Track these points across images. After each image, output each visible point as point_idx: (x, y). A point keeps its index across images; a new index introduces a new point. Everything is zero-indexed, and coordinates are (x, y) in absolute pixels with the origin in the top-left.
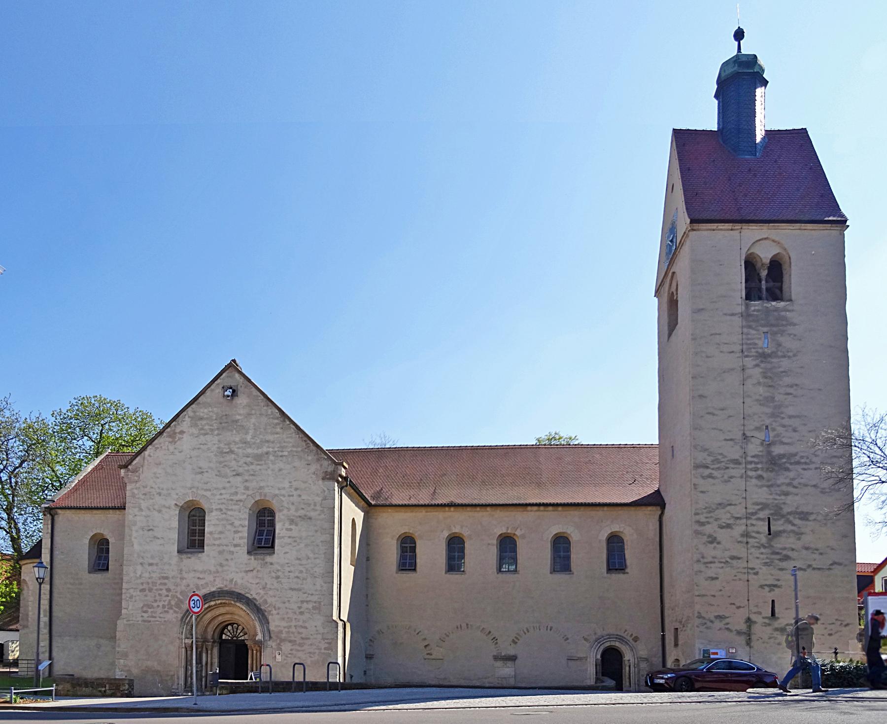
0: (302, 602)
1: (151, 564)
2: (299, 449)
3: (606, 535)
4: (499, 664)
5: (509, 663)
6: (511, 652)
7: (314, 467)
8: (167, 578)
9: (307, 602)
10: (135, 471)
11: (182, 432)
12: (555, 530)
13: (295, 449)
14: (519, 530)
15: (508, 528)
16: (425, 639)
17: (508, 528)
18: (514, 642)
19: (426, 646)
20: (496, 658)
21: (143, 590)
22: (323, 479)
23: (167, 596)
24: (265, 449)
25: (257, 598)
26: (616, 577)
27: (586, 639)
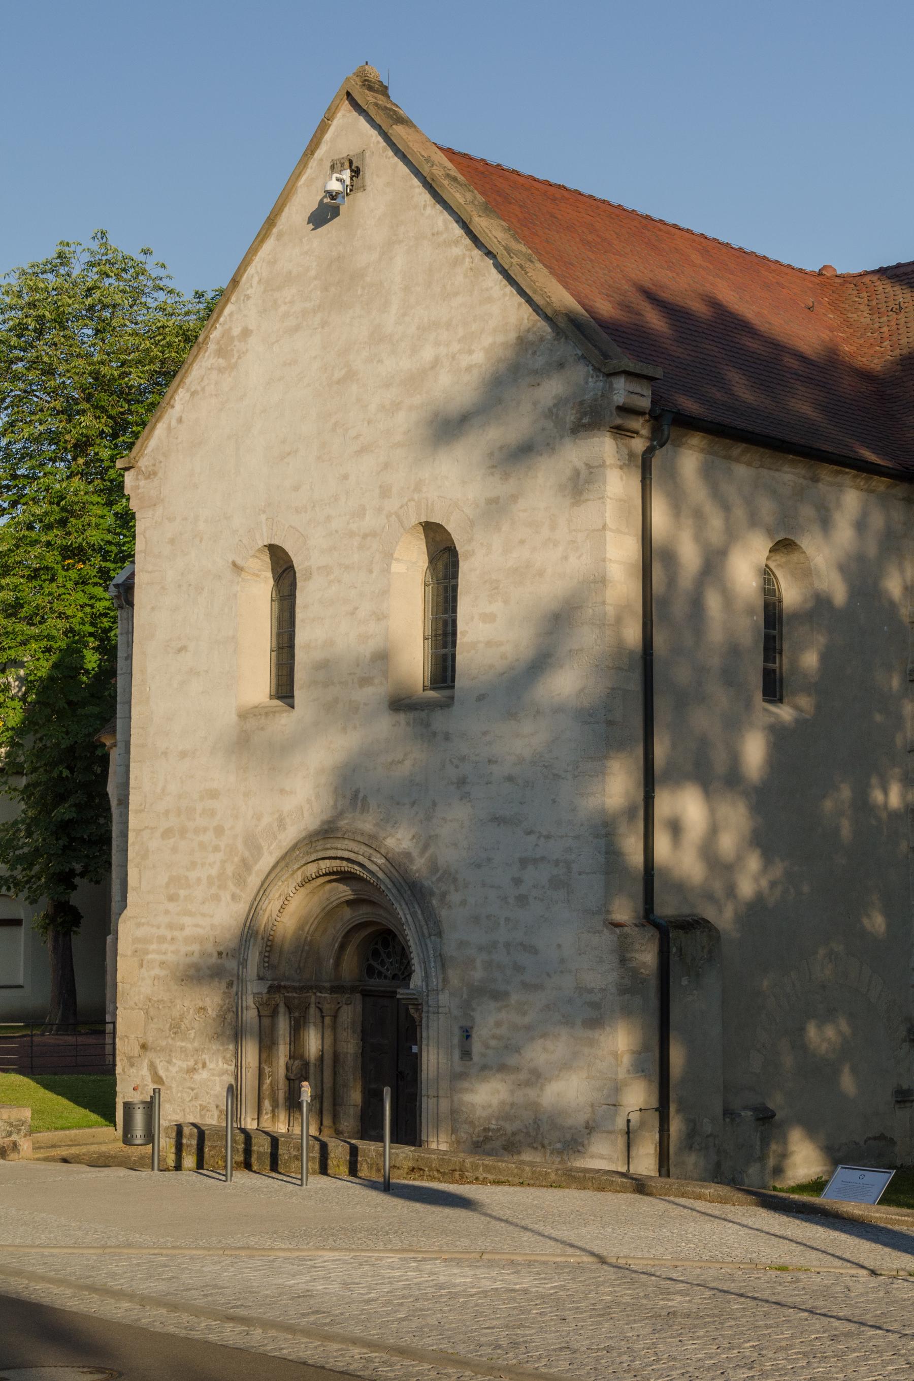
0: (524, 862)
1: (183, 755)
8: (213, 794)
9: (535, 861)
10: (150, 475)
11: (246, 333)
21: (167, 833)
23: (216, 849)
24: (428, 354)
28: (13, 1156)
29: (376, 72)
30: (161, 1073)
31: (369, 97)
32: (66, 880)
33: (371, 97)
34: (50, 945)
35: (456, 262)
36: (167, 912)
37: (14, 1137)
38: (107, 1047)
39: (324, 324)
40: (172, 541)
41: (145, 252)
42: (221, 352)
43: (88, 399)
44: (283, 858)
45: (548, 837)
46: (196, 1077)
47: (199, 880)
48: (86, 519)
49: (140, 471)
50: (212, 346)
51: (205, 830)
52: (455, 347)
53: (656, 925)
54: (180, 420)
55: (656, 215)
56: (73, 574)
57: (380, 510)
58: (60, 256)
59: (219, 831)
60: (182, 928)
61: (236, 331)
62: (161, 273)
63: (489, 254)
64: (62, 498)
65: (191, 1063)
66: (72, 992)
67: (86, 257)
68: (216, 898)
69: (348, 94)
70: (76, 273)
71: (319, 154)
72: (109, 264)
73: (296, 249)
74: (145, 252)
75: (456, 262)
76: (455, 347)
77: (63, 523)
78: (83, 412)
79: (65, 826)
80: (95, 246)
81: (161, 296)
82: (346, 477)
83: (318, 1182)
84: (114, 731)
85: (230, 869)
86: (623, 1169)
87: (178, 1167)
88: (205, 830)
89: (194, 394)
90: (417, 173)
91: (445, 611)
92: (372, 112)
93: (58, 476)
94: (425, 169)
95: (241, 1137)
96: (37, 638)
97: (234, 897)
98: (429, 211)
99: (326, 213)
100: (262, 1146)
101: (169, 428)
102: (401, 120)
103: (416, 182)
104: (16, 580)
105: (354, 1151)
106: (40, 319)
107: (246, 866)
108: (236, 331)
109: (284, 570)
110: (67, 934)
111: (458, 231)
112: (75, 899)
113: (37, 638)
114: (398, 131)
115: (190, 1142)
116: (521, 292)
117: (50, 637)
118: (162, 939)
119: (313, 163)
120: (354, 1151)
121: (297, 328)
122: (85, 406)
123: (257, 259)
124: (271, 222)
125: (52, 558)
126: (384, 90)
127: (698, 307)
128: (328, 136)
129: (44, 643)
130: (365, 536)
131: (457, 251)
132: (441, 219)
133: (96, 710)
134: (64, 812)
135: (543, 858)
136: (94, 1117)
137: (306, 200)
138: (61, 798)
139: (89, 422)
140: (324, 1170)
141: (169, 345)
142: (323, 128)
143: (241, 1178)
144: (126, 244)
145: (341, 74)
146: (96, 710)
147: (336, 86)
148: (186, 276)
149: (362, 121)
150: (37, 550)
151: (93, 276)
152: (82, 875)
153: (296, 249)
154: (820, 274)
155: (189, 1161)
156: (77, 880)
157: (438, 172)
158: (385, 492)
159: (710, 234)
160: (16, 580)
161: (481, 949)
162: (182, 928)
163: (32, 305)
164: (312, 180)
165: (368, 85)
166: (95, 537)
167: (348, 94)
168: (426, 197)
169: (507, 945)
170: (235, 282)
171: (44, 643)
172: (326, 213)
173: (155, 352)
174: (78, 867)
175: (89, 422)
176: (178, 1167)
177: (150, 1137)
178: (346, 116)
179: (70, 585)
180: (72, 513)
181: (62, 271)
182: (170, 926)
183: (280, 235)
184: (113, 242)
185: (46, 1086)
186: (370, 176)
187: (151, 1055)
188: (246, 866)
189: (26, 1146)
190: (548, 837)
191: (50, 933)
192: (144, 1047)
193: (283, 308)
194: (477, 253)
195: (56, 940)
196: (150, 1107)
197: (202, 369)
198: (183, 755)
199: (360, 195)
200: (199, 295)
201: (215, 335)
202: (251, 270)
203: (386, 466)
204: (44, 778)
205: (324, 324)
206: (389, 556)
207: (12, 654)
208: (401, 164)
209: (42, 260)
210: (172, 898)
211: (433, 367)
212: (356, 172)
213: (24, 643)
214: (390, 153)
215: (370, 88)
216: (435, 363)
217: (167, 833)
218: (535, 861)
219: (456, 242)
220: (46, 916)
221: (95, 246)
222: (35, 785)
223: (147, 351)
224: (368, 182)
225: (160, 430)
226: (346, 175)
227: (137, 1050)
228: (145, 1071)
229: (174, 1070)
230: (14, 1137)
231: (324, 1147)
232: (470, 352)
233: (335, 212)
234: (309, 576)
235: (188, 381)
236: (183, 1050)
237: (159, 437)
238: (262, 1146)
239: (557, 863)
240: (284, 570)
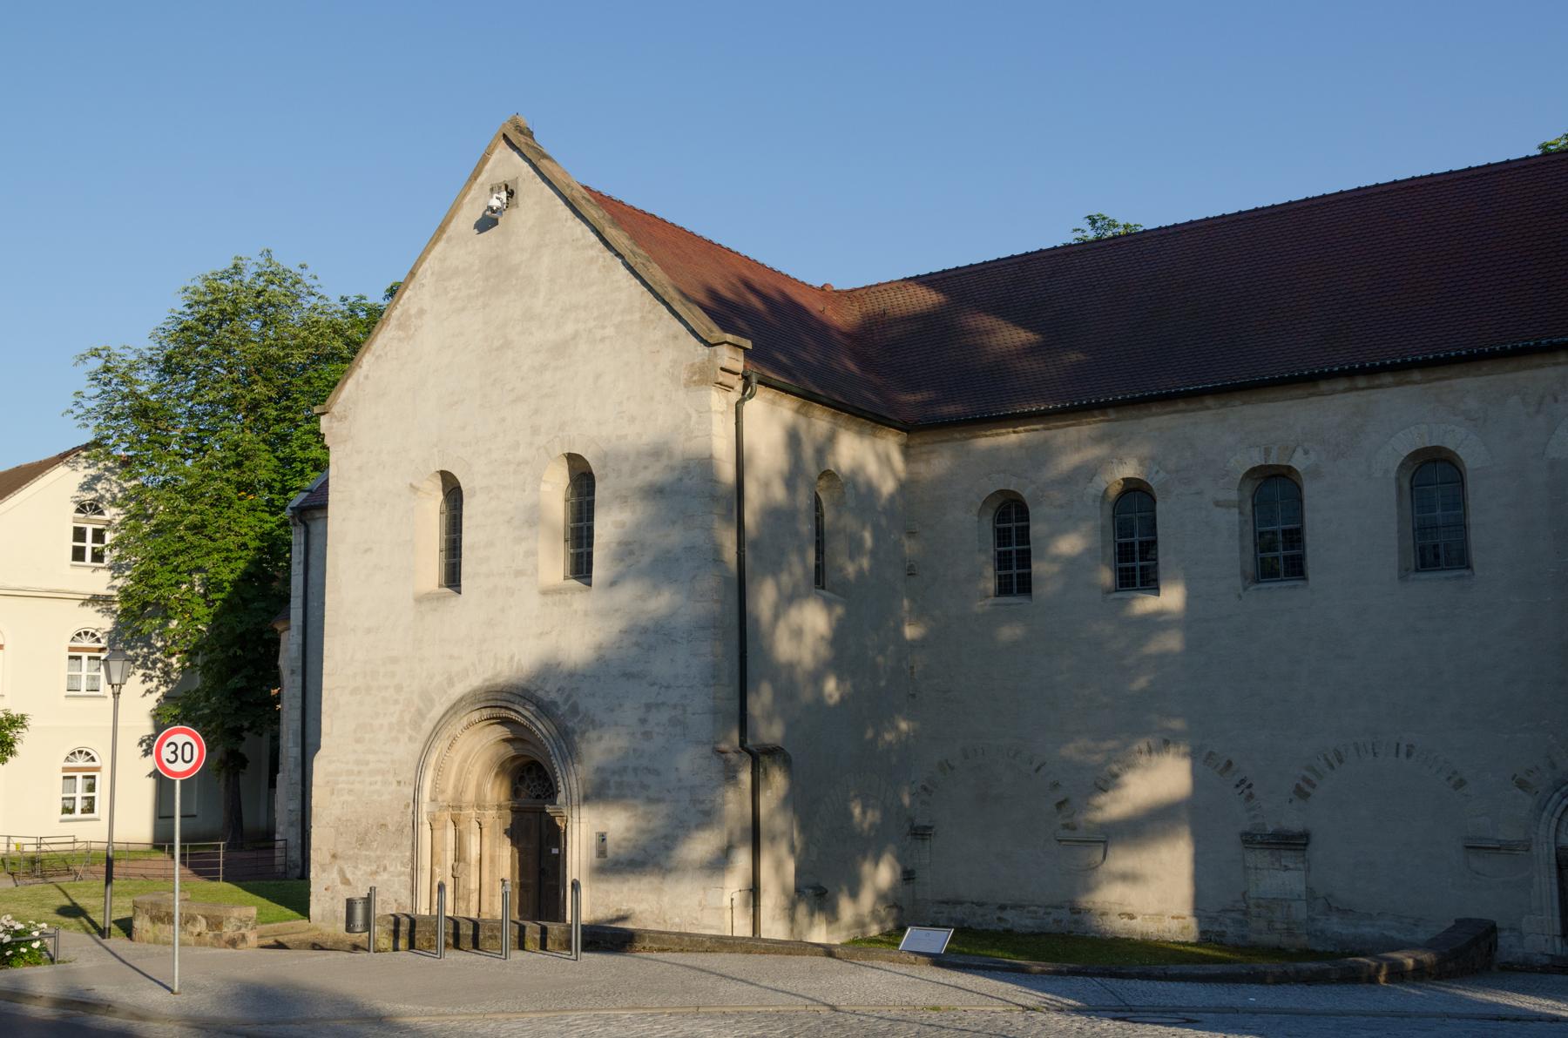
0: (648, 707)
1: (369, 631)
2: (637, 316)
3: (1450, 445)
4: (1260, 858)
5: (1289, 858)
6: (1293, 822)
7: (668, 356)
8: (394, 660)
9: (658, 706)
10: (342, 419)
11: (421, 312)
12: (1407, 442)
13: (628, 318)
14: (1299, 454)
15: (1267, 451)
16: (1056, 785)
17: (1267, 451)
18: (1301, 794)
19: (1060, 805)
20: (1250, 840)
21: (355, 691)
22: (686, 386)
23: (396, 702)
24: (569, 328)
25: (560, 700)
26: (1280, 593)
27: (1522, 785)
28: (242, 945)
29: (525, 121)
30: (349, 876)
31: (519, 139)
32: (237, 733)
33: (522, 138)
34: (222, 782)
35: (592, 261)
36: (355, 752)
37: (243, 930)
38: (277, 853)
39: (485, 306)
40: (360, 468)
41: (302, 267)
42: (401, 326)
43: (258, 371)
44: (452, 708)
45: (668, 687)
46: (379, 878)
47: (381, 726)
48: (257, 461)
49: (333, 416)
50: (393, 322)
51: (387, 688)
52: (592, 324)
53: (750, 752)
54: (367, 377)
55: (716, 241)
56: (246, 503)
57: (531, 444)
58: (235, 267)
59: (399, 688)
60: (367, 763)
61: (413, 311)
62: (314, 282)
63: (618, 255)
64: (238, 446)
65: (374, 868)
66: (240, 819)
67: (255, 269)
68: (396, 740)
69: (505, 136)
70: (247, 280)
71: (480, 179)
72: (274, 276)
73: (463, 248)
74: (302, 267)
75: (592, 261)
76: (592, 324)
77: (238, 465)
78: (255, 382)
79: (238, 693)
80: (262, 261)
81: (314, 300)
82: (503, 420)
83: (518, 955)
84: (288, 618)
85: (407, 718)
86: (743, 929)
87: (396, 949)
88: (387, 688)
89: (378, 357)
90: (561, 195)
91: (580, 520)
92: (524, 150)
93: (237, 430)
94: (567, 193)
95: (451, 925)
96: (218, 550)
97: (411, 739)
98: (570, 223)
99: (487, 223)
100: (467, 930)
101: (358, 384)
102: (545, 156)
103: (559, 201)
104: (202, 507)
105: (544, 931)
106: (222, 312)
107: (421, 714)
108: (413, 311)
109: (453, 493)
110: (236, 774)
111: (593, 238)
112: (243, 749)
113: (218, 550)
114: (544, 164)
115: (404, 929)
116: (644, 283)
117: (228, 550)
118: (350, 773)
119: (476, 187)
120: (544, 931)
121: (463, 309)
122: (257, 377)
123: (433, 253)
124: (442, 229)
125: (230, 492)
126: (530, 134)
127: (777, 297)
128: (488, 166)
129: (224, 554)
130: (519, 464)
131: (592, 253)
132: (580, 229)
133: (263, 605)
134: (236, 682)
135: (663, 704)
136: (289, 912)
137: (471, 212)
138: (234, 672)
139: (260, 389)
140: (521, 946)
141: (322, 335)
142: (484, 160)
143: (453, 956)
144: (287, 260)
145: (501, 121)
146: (263, 605)
147: (496, 129)
148: (334, 284)
149: (515, 155)
150: (218, 484)
151: (260, 284)
152: (249, 730)
153: (463, 248)
154: (823, 288)
155: (402, 943)
156: (245, 734)
157: (576, 194)
158: (535, 431)
159: (752, 256)
160: (202, 507)
161: (614, 773)
162: (367, 763)
163: (214, 301)
164: (475, 199)
165: (520, 130)
166: (264, 475)
167: (505, 136)
168: (568, 212)
169: (635, 770)
170: (412, 274)
171: (224, 554)
172: (487, 223)
173: (312, 339)
174: (246, 724)
175: (260, 389)
176: (396, 949)
177: (367, 926)
178: (502, 151)
179: (243, 511)
180: (247, 458)
181: (236, 278)
182: (358, 762)
183: (449, 239)
184: (275, 259)
185: (247, 889)
186: (520, 195)
187: (340, 862)
188: (421, 714)
189: (252, 938)
190: (668, 687)
191: (223, 775)
192: (334, 856)
193: (452, 294)
194: (609, 254)
195: (227, 780)
196: (368, 901)
197: (385, 338)
198: (369, 631)
199: (513, 211)
200: (344, 299)
201: (396, 313)
202: (425, 265)
203: (536, 412)
204: (222, 656)
205: (485, 306)
206: (539, 479)
207: (199, 562)
208: (547, 188)
209: (221, 269)
210: (358, 741)
211: (574, 338)
212: (511, 194)
213: (208, 554)
214: (539, 180)
215: (521, 132)
216: (575, 336)
217: (355, 691)
218: (658, 706)
219: (592, 246)
220: (220, 760)
221: (262, 261)
222: (213, 661)
223: (304, 339)
224: (520, 202)
225: (350, 385)
226: (504, 195)
227: (328, 859)
228: (335, 875)
229: (359, 873)
230: (243, 930)
231: (522, 929)
232: (604, 327)
233: (495, 222)
234: (473, 494)
235: (373, 347)
236: (367, 857)
237: (349, 391)
238: (467, 930)
239: (675, 707)
240: (453, 493)
